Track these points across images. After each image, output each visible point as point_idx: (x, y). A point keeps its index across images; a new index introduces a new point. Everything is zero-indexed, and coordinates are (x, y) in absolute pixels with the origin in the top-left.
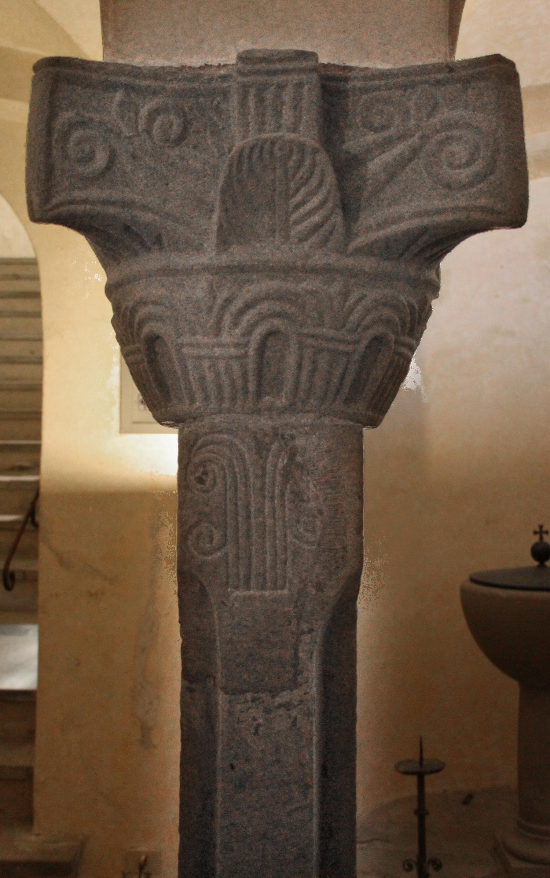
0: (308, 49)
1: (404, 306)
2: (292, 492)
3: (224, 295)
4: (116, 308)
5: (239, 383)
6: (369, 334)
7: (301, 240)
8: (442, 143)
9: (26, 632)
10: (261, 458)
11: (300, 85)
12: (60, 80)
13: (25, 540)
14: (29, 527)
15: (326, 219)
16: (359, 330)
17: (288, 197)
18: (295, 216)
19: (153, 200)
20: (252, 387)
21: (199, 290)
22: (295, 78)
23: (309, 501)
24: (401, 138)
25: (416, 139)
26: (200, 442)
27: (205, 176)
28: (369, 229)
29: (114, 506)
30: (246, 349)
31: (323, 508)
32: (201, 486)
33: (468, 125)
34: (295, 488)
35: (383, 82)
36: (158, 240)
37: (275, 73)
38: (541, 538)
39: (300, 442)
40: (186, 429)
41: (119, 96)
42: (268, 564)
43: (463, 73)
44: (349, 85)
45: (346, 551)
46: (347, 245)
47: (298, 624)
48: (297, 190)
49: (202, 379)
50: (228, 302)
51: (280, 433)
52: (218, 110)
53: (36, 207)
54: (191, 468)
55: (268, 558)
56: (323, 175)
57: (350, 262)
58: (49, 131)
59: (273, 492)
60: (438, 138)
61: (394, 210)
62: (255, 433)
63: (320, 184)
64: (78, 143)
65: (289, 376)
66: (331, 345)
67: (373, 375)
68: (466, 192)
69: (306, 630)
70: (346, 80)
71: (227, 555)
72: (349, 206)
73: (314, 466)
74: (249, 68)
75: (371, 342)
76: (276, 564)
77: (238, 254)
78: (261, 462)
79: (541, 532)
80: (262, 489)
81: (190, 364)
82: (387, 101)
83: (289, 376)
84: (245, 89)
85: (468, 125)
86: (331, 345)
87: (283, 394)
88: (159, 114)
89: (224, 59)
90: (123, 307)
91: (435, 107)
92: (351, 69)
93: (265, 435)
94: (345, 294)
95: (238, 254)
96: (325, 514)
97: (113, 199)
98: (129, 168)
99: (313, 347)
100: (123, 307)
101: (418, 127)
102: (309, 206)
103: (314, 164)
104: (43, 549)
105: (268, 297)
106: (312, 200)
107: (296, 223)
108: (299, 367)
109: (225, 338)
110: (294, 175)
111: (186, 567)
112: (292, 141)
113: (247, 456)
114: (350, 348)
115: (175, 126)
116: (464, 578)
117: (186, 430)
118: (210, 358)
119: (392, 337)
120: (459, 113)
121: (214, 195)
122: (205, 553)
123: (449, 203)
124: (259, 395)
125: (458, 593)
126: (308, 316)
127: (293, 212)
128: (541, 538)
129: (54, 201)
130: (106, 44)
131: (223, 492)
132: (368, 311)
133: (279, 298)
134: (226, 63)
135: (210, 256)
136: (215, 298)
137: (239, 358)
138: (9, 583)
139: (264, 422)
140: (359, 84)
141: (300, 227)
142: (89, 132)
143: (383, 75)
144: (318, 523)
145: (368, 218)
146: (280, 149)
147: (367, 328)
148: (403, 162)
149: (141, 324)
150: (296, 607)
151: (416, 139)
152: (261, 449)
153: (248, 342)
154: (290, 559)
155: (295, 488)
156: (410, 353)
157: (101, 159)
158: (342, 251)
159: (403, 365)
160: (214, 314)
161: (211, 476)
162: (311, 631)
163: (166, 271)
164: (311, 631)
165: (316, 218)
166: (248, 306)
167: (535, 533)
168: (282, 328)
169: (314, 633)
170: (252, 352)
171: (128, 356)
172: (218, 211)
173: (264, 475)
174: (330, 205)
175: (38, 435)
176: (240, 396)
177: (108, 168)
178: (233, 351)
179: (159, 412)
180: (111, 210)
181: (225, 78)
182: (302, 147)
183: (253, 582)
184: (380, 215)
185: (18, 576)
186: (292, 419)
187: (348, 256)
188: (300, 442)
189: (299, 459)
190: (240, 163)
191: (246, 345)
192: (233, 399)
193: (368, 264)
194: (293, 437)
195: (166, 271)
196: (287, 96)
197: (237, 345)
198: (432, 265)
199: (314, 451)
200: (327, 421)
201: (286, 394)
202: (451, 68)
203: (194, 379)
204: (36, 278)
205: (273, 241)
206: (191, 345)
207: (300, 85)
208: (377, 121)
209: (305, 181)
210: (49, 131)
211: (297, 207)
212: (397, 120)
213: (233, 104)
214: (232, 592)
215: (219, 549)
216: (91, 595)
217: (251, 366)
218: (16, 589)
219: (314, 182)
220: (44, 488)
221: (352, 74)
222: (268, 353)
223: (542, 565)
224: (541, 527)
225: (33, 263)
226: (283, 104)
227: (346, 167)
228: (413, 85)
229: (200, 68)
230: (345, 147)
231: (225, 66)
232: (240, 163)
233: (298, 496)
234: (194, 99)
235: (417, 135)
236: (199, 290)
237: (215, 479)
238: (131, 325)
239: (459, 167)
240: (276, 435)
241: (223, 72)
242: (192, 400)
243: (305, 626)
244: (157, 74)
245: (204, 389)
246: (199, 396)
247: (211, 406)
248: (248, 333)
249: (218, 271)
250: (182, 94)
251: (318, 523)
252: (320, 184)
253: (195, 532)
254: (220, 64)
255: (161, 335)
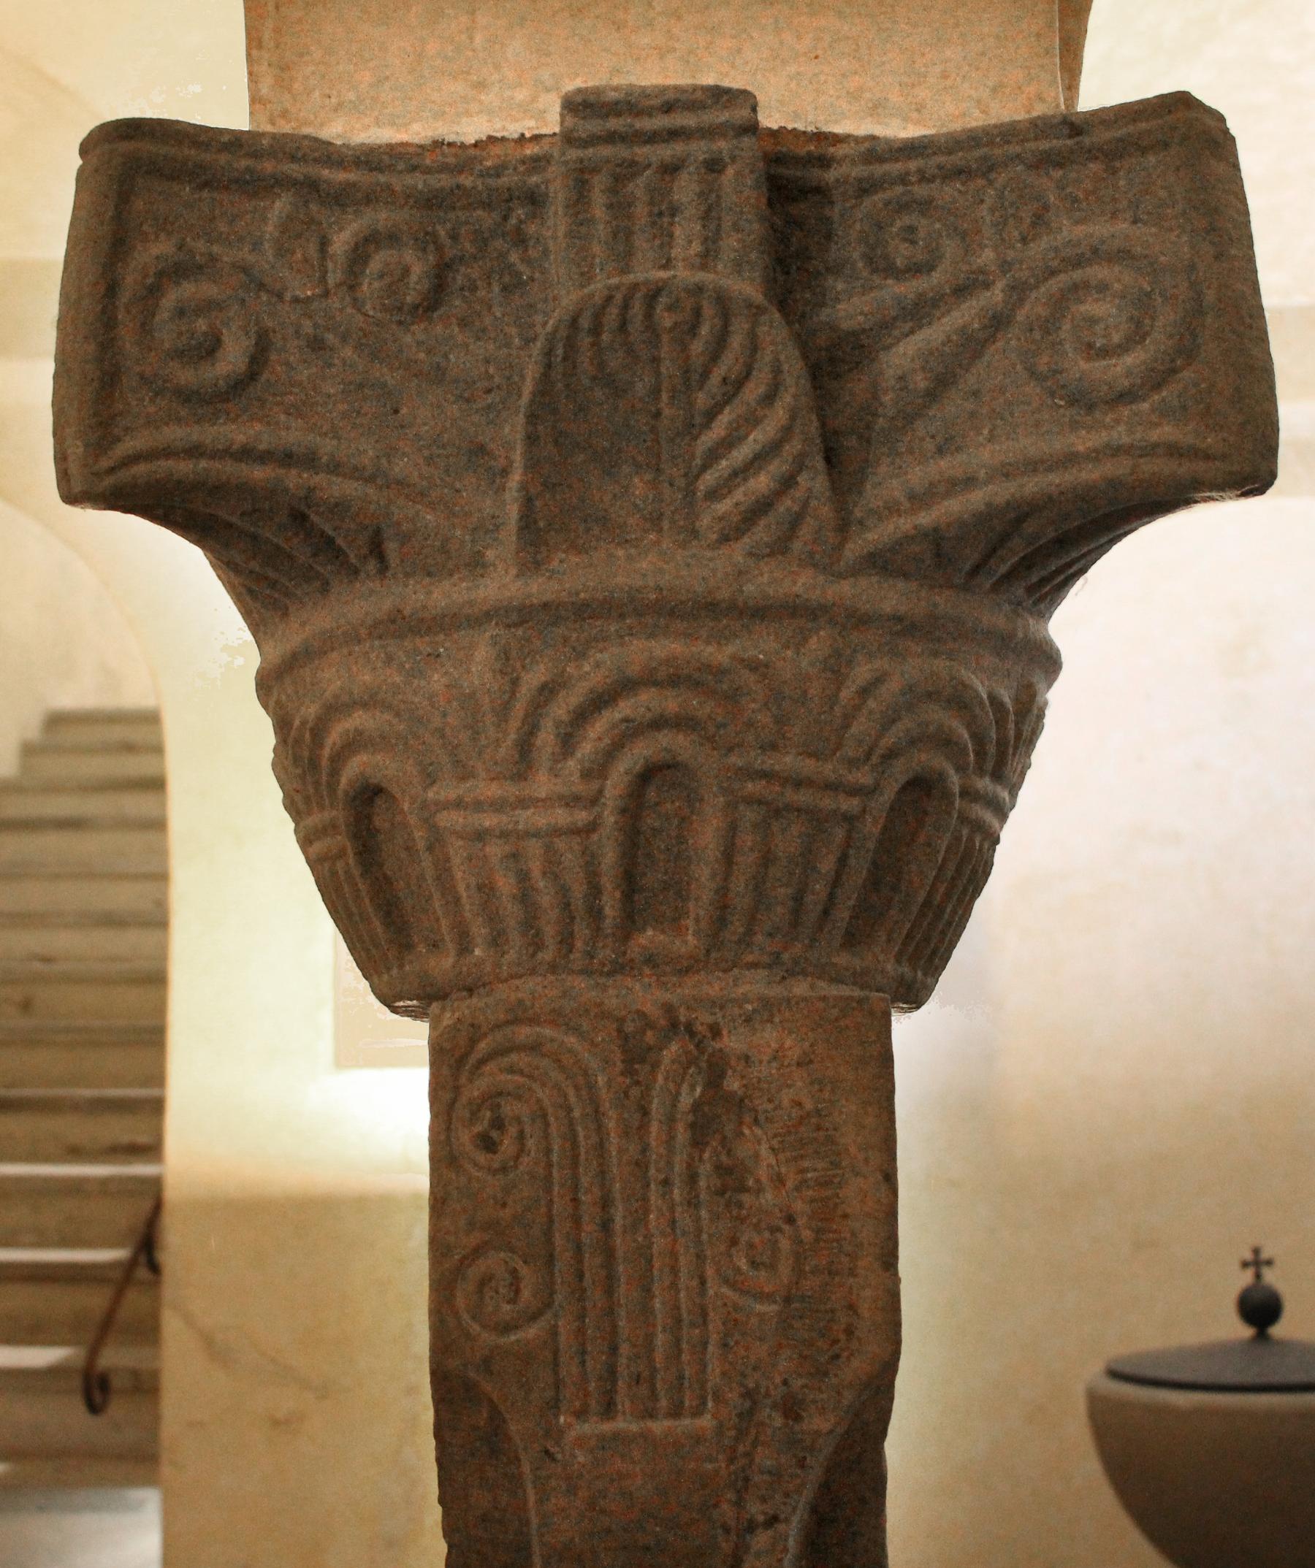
0: (734, 82)
1: (981, 703)
2: (718, 1168)
3: (534, 678)
4: (282, 726)
5: (578, 892)
6: (900, 772)
7: (725, 539)
8: (1060, 303)
9: (138, 1507)
10: (638, 1083)
11: (714, 166)
12: (138, 169)
13: (134, 1300)
14: (142, 1273)
15: (788, 482)
16: (874, 759)
17: (691, 429)
18: (709, 479)
19: (366, 451)
20: (611, 906)
21: (479, 660)
22: (699, 150)
23: (759, 1191)
24: (961, 291)
25: (996, 295)
26: (483, 1046)
27: (489, 391)
28: (893, 509)
29: (300, 1224)
30: (597, 809)
31: (799, 1206)
32: (490, 1156)
33: (1123, 255)
34: (724, 1158)
35: (913, 165)
36: (376, 549)
37: (653, 138)
38: (1258, 1276)
39: (732, 1042)
40: (448, 1015)
41: (280, 206)
42: (659, 1356)
43: (1108, 135)
44: (831, 175)
45: (856, 1313)
46: (839, 547)
47: (739, 1504)
48: (711, 415)
49: (486, 890)
50: (546, 693)
51: (682, 1019)
52: (520, 239)
53: (74, 468)
54: (461, 1111)
55: (661, 1339)
56: (777, 371)
57: (844, 590)
58: (112, 290)
59: (669, 1164)
60: (1055, 284)
61: (947, 466)
62: (621, 1020)
63: (769, 398)
64: (181, 312)
65: (704, 875)
66: (803, 797)
67: (905, 876)
68: (1126, 412)
69: (761, 1518)
70: (824, 162)
71: (554, 1332)
72: (841, 453)
73: (770, 1101)
74: (594, 126)
75: (904, 789)
76: (680, 1351)
77: (572, 575)
78: (635, 1092)
79: (1257, 1262)
80: (641, 1165)
81: (457, 851)
82: (925, 206)
83: (704, 875)
84: (581, 177)
85: (1123, 255)
86: (803, 797)
87: (690, 923)
88: (378, 248)
89: (532, 123)
90: (297, 723)
91: (1040, 220)
92: (837, 139)
93: (649, 1024)
94: (836, 668)
95: (572, 575)
96: (801, 1222)
97: (262, 447)
98: (304, 374)
99: (760, 802)
100: (297, 723)
101: (1005, 266)
102: (742, 453)
103: (754, 347)
104: (171, 1324)
105: (649, 679)
106: (751, 437)
107: (714, 494)
108: (728, 856)
109: (542, 784)
110: (705, 374)
111: (453, 1363)
112: (699, 289)
113: (601, 1080)
114: (850, 804)
115: (414, 278)
116: (1093, 1371)
117: (448, 1019)
118: (504, 835)
119: (955, 781)
120: (1100, 229)
121: (514, 429)
122: (507, 1328)
123: (1083, 442)
124: (631, 921)
125: (1081, 1407)
126: (750, 724)
127: (705, 468)
128: (1258, 1276)
129: (121, 450)
130: (255, 100)
131: (541, 1171)
132: (889, 721)
133: (674, 681)
134: (536, 132)
135: (501, 584)
136: (515, 683)
137: (574, 831)
138: (98, 1398)
139: (644, 995)
140: (858, 171)
141: (723, 507)
142: (209, 290)
143: (912, 149)
144: (785, 1244)
145: (890, 481)
146: (670, 308)
147: (891, 755)
148: (971, 346)
149: (339, 758)
150: (731, 1460)
151: (996, 295)
152: (636, 1057)
153: (600, 792)
154: (714, 1338)
155: (724, 1158)
156: (996, 823)
157: (233, 357)
158: (828, 565)
159: (980, 850)
160: (514, 724)
161: (513, 1130)
162: (773, 1520)
163: (398, 626)
164: (773, 1520)
165: (762, 482)
166: (599, 701)
167: (1245, 1265)
168: (684, 756)
169: (781, 1527)
170: (610, 819)
171: (311, 842)
172: (520, 471)
173: (643, 1127)
174: (793, 447)
175: (157, 1077)
176: (582, 931)
177: (252, 374)
178: (561, 817)
179: (385, 977)
180: (259, 474)
181: (537, 163)
182: (723, 302)
183: (623, 1401)
184: (918, 475)
185: (116, 1382)
186: (713, 986)
187: (841, 576)
188: (732, 1042)
189: (733, 1084)
190: (570, 345)
191: (595, 800)
192: (566, 941)
193: (891, 597)
194: (715, 1031)
195: (398, 626)
196: (685, 189)
197: (572, 801)
198: (1042, 606)
199: (769, 1062)
200: (800, 988)
201: (697, 920)
202: (1075, 126)
203: (468, 887)
204: (158, 750)
205: (658, 543)
206: (459, 804)
207: (714, 166)
208: (902, 253)
209: (735, 386)
210: (112, 290)
211: (713, 456)
212: (950, 247)
213: (556, 224)
214: (570, 1426)
215: (534, 1317)
216: (276, 1423)
217: (609, 858)
218: (117, 1408)
219: (753, 391)
220: (173, 1193)
221: (840, 150)
222: (651, 821)
223: (1262, 1334)
224: (1256, 1251)
225: (151, 719)
226: (674, 211)
227: (833, 363)
228: (988, 168)
229: (476, 145)
230: (824, 315)
231: (536, 138)
232: (570, 345)
233: (732, 1180)
234: (458, 213)
235: (1000, 285)
236: (479, 660)
237: (521, 1136)
238: (314, 764)
239: (1105, 353)
240: (674, 1025)
241: (530, 150)
242: (464, 948)
243: (755, 1509)
244: (370, 158)
245: (493, 918)
246: (479, 930)
247: (512, 955)
248: (597, 771)
249: (522, 616)
250: (432, 202)
251: (785, 1244)
252: (769, 398)
253: (474, 1272)
254: (523, 135)
255: (384, 785)
